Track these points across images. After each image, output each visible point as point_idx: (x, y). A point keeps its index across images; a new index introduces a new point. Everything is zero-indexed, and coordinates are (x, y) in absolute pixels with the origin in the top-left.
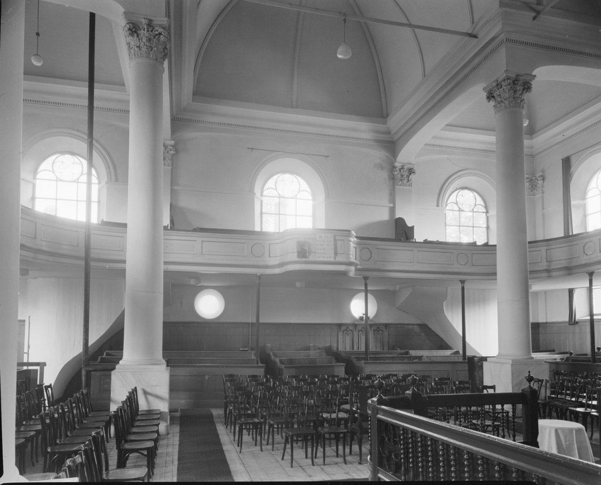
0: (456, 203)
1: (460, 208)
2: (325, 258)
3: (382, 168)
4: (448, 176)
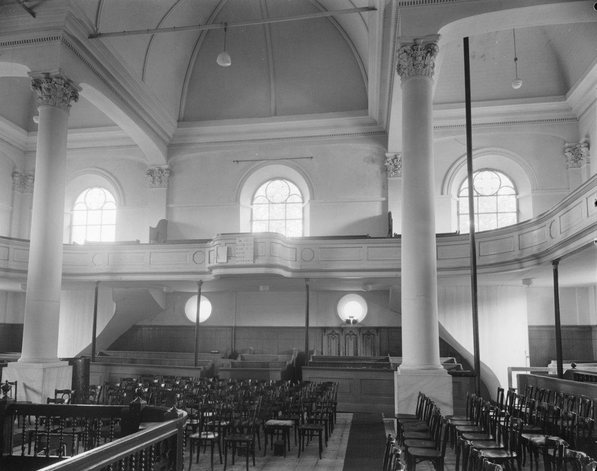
0: (85, 203)
1: (269, 201)
2: (243, 261)
3: (373, 161)
4: (446, 170)
